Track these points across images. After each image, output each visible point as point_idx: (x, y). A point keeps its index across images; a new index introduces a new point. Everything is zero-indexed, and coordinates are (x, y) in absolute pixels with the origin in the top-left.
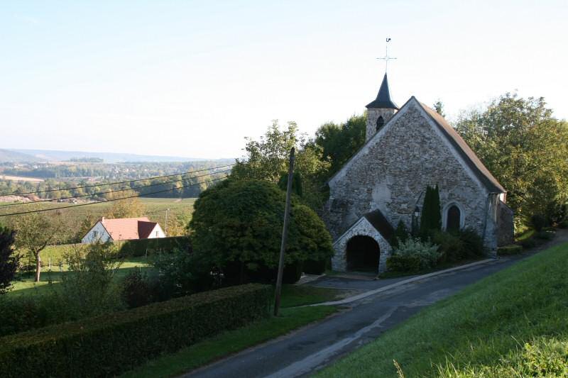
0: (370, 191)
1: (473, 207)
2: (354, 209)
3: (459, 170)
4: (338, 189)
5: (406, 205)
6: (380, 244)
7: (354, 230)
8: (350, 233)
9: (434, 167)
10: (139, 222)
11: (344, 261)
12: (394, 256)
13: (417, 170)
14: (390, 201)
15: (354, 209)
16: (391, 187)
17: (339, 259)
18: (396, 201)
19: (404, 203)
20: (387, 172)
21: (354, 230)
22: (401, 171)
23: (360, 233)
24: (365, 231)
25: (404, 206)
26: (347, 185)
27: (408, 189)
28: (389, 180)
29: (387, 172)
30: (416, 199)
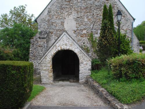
0: (62, 23)
1: (125, 29)
2: (54, 36)
3: (115, 6)
4: (43, 24)
5: (86, 30)
6: (80, 55)
7: (57, 45)
8: (54, 48)
9: (101, 5)
10: (27, 60)
11: (51, 74)
12: (85, 67)
13: (91, 7)
14: (76, 29)
15: (54, 36)
16: (76, 20)
17: (47, 72)
18: (79, 29)
19: (85, 29)
20: (73, 10)
21: (57, 45)
22: (81, 9)
23: (63, 48)
24: (66, 45)
25: (84, 32)
26: (49, 21)
27: (86, 20)
28: (74, 15)
29: (73, 10)
30: (92, 26)
